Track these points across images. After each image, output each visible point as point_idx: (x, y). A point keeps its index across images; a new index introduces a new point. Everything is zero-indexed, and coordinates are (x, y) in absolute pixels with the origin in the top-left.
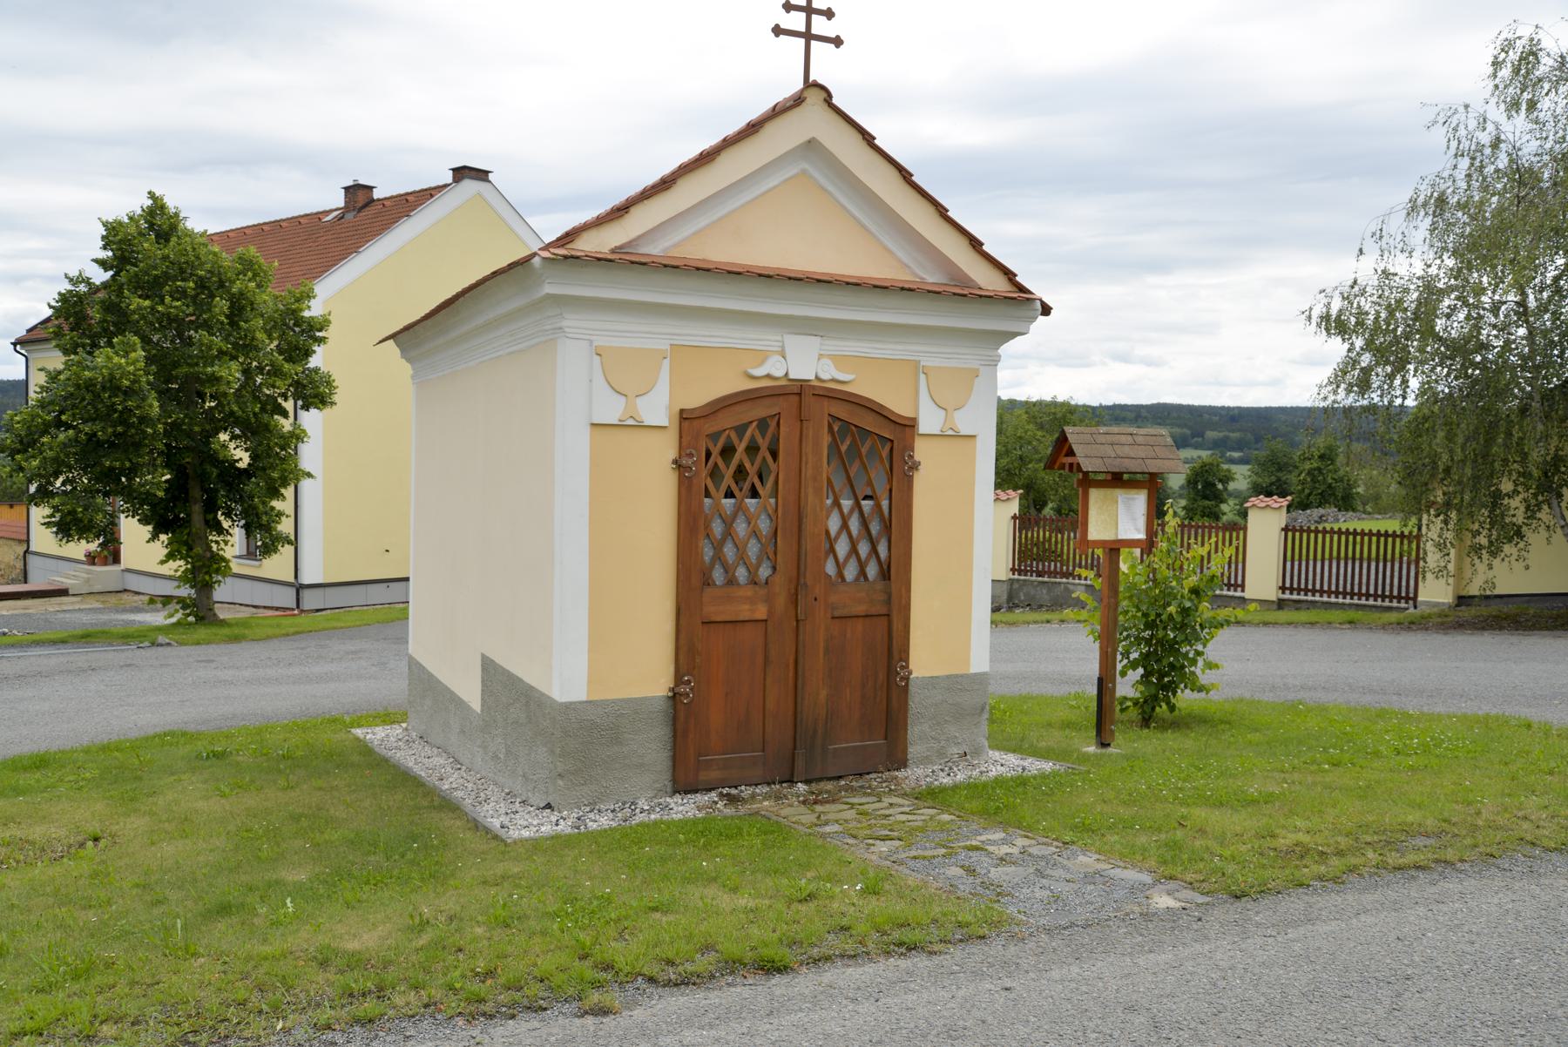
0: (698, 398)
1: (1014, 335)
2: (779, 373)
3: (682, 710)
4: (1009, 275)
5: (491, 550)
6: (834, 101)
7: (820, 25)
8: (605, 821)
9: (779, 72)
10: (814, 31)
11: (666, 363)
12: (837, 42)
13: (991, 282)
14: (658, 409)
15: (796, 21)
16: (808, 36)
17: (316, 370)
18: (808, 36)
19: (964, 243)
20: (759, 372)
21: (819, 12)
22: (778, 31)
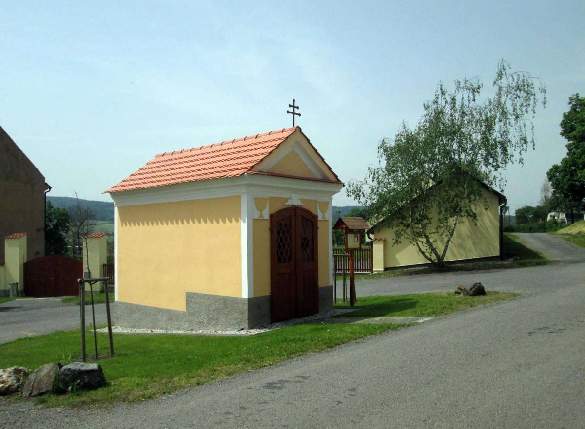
0: (274, 211)
1: (336, 193)
2: (290, 204)
3: (253, 303)
4: (336, 176)
5: (187, 271)
6: (302, 131)
7: (297, 111)
8: (384, 209)
9: (287, 123)
10: (295, 112)
11: (268, 201)
12: (299, 115)
13: (332, 178)
14: (266, 216)
15: (291, 109)
16: (294, 113)
17: (561, 163)
18: (294, 113)
19: (327, 168)
20: (287, 204)
21: (296, 107)
22: (288, 112)
